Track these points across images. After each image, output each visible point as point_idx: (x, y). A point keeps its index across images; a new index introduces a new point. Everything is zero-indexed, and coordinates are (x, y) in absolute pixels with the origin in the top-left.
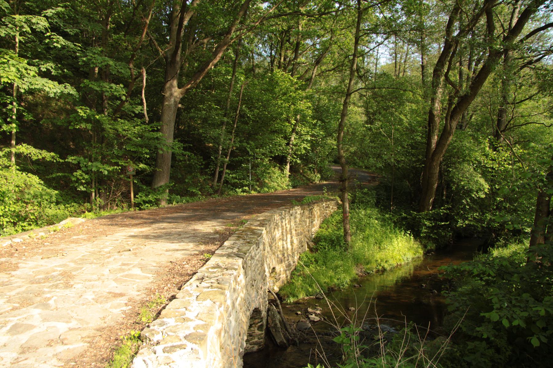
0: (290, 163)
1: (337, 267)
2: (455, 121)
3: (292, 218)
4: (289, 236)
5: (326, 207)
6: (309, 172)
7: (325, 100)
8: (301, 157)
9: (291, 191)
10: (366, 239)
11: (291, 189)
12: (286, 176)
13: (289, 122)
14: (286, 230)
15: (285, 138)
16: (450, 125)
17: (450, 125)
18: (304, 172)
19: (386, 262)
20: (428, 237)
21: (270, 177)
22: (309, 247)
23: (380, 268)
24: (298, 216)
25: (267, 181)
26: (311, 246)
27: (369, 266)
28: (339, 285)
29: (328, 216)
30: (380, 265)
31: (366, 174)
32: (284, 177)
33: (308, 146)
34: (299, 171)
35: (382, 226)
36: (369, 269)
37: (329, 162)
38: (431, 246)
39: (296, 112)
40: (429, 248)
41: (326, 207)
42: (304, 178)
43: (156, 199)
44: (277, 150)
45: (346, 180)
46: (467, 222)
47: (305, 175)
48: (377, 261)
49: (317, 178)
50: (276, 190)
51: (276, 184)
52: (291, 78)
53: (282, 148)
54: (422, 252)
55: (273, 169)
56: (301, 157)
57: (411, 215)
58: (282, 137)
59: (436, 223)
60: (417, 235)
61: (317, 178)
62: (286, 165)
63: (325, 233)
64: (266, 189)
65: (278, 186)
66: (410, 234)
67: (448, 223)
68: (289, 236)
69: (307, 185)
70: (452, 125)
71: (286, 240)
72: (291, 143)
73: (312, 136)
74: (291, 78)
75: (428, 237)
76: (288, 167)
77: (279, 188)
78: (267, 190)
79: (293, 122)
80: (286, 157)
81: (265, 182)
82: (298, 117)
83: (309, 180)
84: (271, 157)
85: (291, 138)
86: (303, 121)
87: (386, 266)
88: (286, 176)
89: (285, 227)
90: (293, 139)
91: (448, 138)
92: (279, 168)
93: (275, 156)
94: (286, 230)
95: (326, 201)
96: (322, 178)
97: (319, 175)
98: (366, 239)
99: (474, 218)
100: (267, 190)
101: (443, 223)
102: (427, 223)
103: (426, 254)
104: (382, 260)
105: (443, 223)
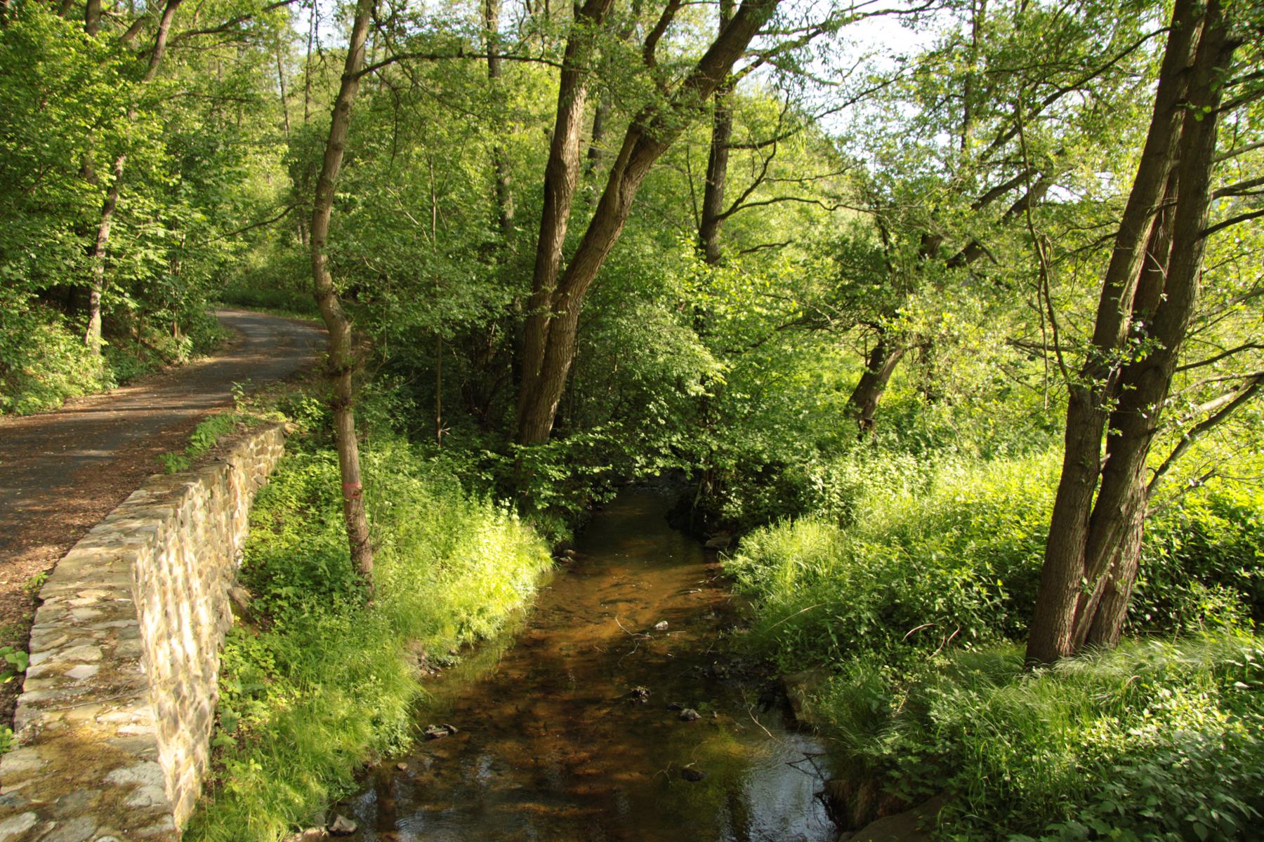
0: (104, 308)
1: (354, 675)
2: (633, 183)
3: (186, 530)
4: (185, 606)
5: (258, 453)
6: (157, 333)
7: (193, 122)
8: (137, 289)
9: (118, 400)
10: (404, 546)
11: (116, 391)
12: (94, 351)
13: (94, 179)
14: (175, 591)
15: (80, 230)
16: (621, 194)
17: (621, 194)
18: (142, 333)
19: (481, 611)
20: (554, 509)
21: (41, 356)
22: (237, 609)
23: (469, 636)
24: (200, 515)
25: (30, 370)
26: (245, 605)
27: (437, 639)
28: (382, 743)
29: (264, 481)
30: (469, 628)
31: (309, 330)
32: (86, 354)
33: (157, 255)
34: (128, 330)
35: (437, 493)
36: (440, 648)
37: (211, 299)
38: (562, 534)
39: (118, 147)
40: (559, 539)
41: (258, 453)
42: (148, 352)
43: (112, 40)
44: (59, 269)
45: (346, 369)
46: (660, 462)
47: (147, 341)
48: (454, 614)
49: (182, 349)
50: (66, 397)
51: (64, 378)
52: (89, 38)
53: (73, 264)
54: (548, 555)
55: (46, 328)
56: (137, 289)
57: (512, 455)
58: (70, 229)
59: (574, 471)
60: (525, 509)
61: (182, 349)
62: (90, 315)
63: (277, 546)
64: (34, 400)
65: (71, 382)
66: (509, 509)
67: (610, 467)
68: (185, 606)
69: (159, 370)
70: (626, 193)
71: (179, 630)
72: (101, 246)
73: (171, 224)
74: (89, 38)
75: (554, 509)
76: (97, 321)
77: (75, 391)
78: (39, 402)
79: (106, 177)
80: (88, 291)
81: (24, 374)
82: (121, 164)
83: (159, 354)
84: (39, 291)
85: (99, 230)
86: (136, 176)
87: (480, 624)
88: (94, 351)
89: (169, 584)
90: (106, 233)
91: (612, 231)
92: (66, 324)
93: (52, 288)
94: (175, 591)
95: (255, 433)
96: (201, 348)
97: (188, 341)
98: (404, 546)
99: (673, 448)
100: (39, 402)
101: (596, 470)
102: (555, 473)
103: (558, 553)
104: (468, 609)
105: (596, 470)
